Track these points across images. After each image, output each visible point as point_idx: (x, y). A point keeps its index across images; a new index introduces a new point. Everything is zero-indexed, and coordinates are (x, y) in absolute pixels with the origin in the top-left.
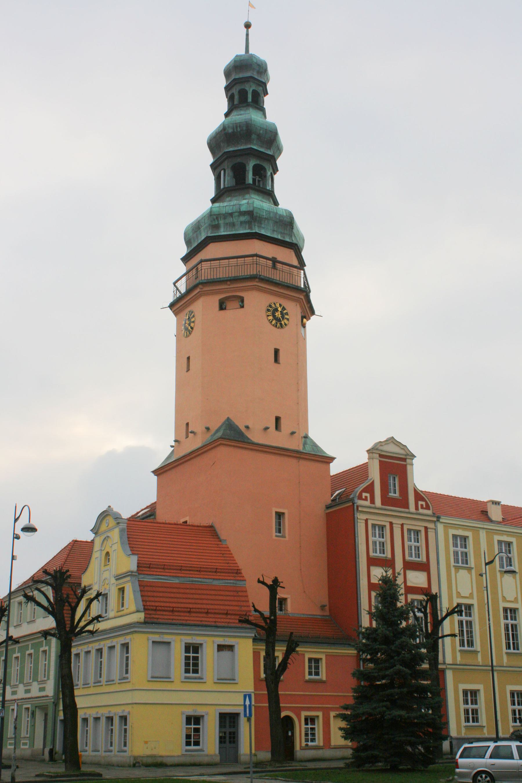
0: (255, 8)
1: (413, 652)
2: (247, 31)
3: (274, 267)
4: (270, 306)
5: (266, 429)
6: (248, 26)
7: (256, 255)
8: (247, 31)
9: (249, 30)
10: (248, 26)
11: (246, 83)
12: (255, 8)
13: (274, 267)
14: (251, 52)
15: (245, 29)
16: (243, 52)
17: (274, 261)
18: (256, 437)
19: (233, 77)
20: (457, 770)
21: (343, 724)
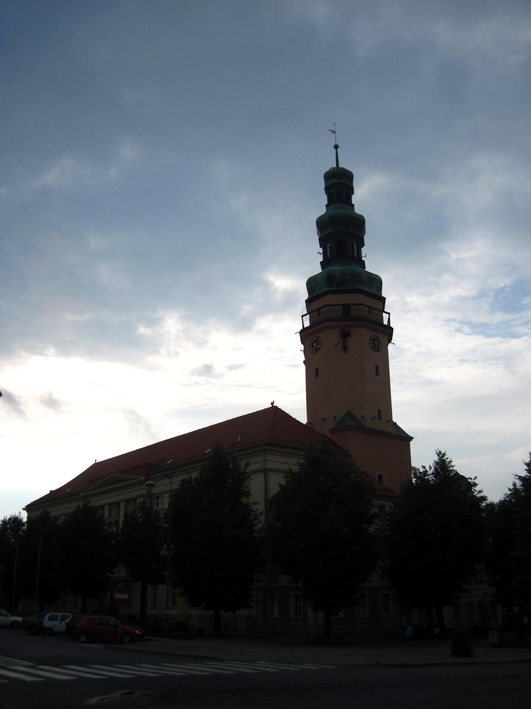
0: (345, 352)
1: (113, 542)
2: (337, 151)
3: (370, 311)
4: (371, 337)
5: (374, 418)
6: (336, 147)
7: (362, 304)
8: (337, 151)
9: (338, 150)
10: (336, 147)
11: (339, 185)
12: (345, 352)
13: (370, 311)
14: (340, 166)
15: (335, 150)
16: (335, 166)
17: (370, 308)
18: (369, 424)
19: (332, 181)
20: (255, 528)
21: (81, 507)
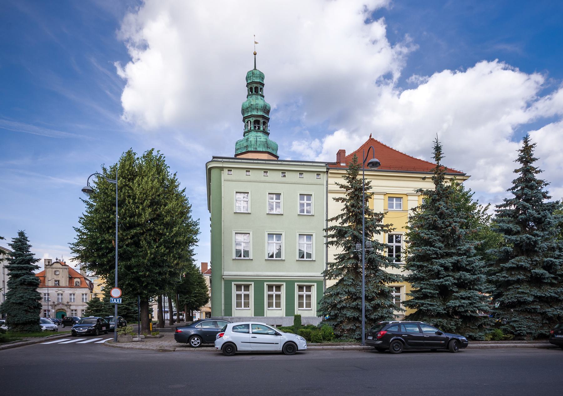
6: (255, 54)
